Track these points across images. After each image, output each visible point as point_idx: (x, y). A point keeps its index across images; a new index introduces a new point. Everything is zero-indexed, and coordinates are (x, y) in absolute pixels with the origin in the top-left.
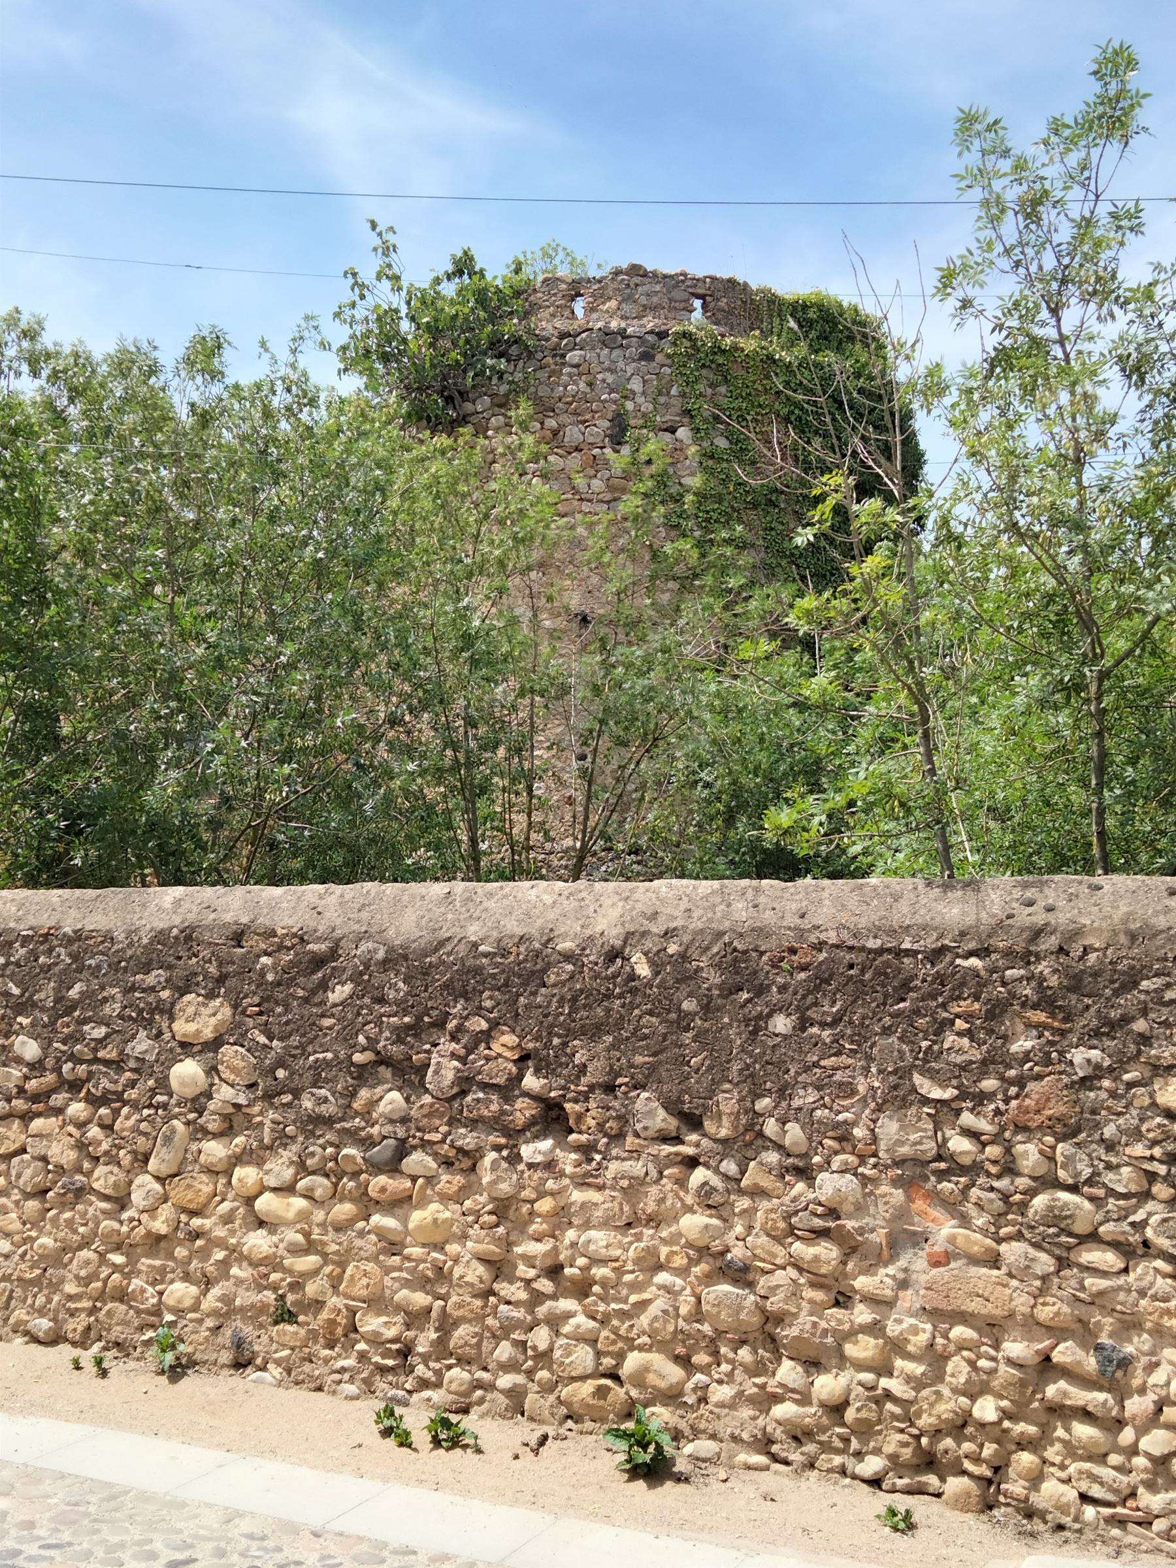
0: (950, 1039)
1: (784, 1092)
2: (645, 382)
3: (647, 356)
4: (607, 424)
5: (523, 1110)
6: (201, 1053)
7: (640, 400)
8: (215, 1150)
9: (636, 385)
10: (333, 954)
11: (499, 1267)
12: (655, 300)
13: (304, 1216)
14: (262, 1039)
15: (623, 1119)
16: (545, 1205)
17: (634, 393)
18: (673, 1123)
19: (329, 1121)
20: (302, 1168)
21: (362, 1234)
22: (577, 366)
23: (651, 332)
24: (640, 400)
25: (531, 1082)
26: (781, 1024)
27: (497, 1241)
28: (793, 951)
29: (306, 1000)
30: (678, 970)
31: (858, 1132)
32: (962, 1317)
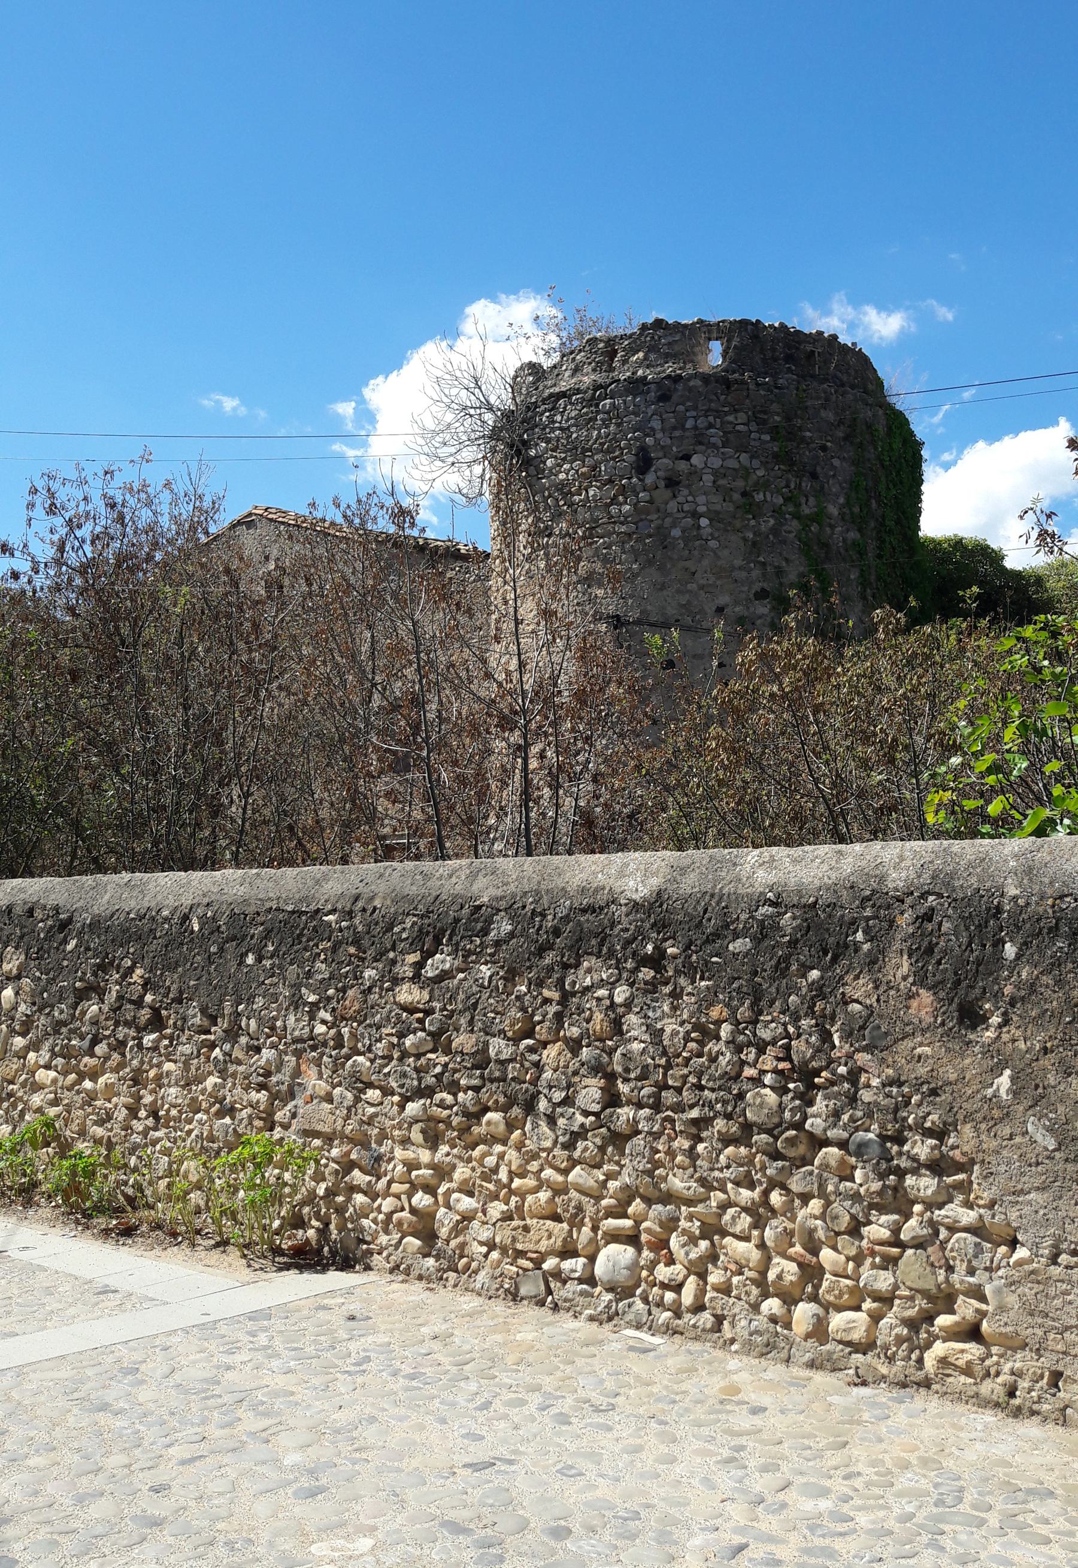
0: (318, 964)
1: (250, 1000)
2: (663, 421)
3: (664, 398)
4: (633, 458)
5: (145, 1014)
6: (892, 984)
7: (659, 435)
8: (19, 1042)
9: (656, 424)
10: (70, 920)
11: (133, 1111)
12: (677, 348)
13: (54, 1081)
14: (38, 974)
15: (184, 1019)
16: (152, 1073)
17: (653, 429)
18: (206, 1023)
19: (64, 1024)
20: (54, 1055)
21: (78, 1092)
22: (608, 413)
23: (669, 377)
24: (659, 435)
25: (149, 998)
26: (250, 959)
27: (132, 1096)
28: (258, 914)
29: (58, 949)
30: (210, 925)
31: (279, 1024)
32: (316, 1134)
